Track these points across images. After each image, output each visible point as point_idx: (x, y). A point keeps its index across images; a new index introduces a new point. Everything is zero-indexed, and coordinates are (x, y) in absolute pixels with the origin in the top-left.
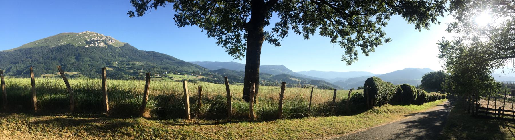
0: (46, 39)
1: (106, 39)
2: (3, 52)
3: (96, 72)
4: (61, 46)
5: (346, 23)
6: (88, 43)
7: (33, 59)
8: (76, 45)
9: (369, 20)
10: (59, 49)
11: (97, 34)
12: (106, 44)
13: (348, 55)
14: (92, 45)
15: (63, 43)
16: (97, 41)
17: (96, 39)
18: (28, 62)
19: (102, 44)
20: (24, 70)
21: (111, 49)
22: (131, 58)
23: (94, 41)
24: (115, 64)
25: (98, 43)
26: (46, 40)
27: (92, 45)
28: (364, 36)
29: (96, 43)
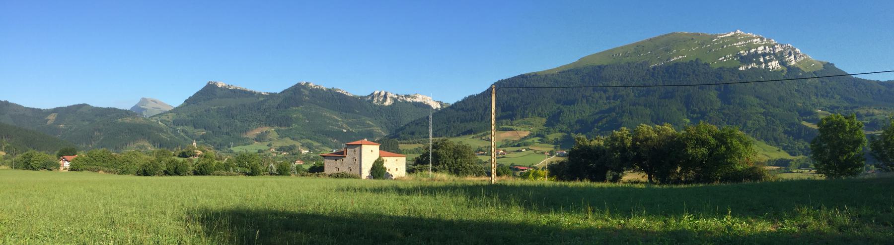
0: (638, 45)
1: (781, 52)
2: (535, 75)
3: (786, 132)
4: (676, 64)
7: (611, 92)
8: (715, 65)
10: (673, 70)
11: (762, 39)
12: (783, 63)
14: (754, 65)
16: (764, 55)
18: (601, 102)
19: (774, 64)
20: (596, 121)
23: (756, 55)
24: (821, 114)
25: (766, 62)
26: (639, 47)
27: (754, 65)
29: (762, 60)
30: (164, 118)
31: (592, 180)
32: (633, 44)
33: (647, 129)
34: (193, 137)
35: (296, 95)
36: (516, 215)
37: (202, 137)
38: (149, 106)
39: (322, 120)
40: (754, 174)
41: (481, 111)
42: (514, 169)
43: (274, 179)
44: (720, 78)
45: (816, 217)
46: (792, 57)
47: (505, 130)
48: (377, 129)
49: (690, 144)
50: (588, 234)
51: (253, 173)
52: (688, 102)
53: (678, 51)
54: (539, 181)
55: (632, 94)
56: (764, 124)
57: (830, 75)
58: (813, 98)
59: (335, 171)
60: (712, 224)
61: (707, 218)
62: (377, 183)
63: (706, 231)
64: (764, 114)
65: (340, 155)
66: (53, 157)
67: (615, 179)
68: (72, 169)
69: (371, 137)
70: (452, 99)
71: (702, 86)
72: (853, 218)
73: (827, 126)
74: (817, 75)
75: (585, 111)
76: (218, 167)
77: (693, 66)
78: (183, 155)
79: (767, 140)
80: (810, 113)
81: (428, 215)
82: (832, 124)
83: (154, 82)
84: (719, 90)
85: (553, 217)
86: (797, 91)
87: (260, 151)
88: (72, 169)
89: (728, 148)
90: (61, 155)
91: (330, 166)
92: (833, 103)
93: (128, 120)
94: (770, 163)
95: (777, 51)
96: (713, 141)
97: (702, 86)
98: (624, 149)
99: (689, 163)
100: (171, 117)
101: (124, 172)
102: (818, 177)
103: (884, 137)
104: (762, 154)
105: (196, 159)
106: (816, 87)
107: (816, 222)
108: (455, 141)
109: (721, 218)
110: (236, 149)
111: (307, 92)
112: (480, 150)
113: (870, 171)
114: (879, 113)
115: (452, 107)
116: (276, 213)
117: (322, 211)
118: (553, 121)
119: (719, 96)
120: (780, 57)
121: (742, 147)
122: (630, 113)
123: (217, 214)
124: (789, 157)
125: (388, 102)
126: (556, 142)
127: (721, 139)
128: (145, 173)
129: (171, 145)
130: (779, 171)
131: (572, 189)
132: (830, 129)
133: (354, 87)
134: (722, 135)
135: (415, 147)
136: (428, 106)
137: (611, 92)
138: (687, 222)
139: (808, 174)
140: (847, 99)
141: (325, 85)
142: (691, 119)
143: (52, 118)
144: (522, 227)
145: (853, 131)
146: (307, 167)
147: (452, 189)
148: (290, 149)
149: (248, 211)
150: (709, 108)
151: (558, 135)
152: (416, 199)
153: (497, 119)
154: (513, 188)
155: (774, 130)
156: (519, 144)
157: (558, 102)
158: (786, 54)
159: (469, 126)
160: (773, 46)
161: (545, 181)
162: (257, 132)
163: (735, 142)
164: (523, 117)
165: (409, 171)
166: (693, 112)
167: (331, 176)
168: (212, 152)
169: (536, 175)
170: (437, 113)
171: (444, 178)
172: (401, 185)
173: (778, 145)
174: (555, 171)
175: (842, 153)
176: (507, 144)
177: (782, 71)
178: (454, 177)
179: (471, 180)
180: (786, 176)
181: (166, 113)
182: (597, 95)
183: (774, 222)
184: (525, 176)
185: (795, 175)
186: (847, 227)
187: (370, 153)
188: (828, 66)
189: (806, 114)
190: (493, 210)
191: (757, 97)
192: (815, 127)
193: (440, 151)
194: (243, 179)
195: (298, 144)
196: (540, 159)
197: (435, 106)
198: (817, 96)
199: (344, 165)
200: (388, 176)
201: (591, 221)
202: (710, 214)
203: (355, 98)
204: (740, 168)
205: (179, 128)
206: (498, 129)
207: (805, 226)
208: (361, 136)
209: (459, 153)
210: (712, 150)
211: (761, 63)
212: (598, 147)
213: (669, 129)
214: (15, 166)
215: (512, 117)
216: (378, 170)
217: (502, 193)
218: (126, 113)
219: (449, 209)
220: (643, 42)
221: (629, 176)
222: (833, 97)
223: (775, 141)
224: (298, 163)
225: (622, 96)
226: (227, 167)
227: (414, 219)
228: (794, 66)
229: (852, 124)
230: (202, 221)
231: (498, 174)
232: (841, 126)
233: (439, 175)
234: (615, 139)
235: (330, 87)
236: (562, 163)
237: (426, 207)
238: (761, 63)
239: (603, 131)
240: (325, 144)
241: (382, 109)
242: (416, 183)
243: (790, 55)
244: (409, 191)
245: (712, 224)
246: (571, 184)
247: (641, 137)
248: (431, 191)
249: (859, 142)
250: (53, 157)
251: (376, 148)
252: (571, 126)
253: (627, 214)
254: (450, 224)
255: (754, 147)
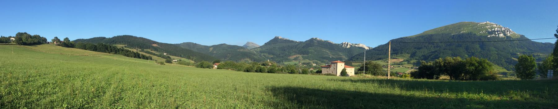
0: (446, 27)
2: (406, 38)
3: (505, 62)
4: (463, 34)
5: (125, 48)
6: (490, 33)
7: (435, 45)
8: (478, 34)
10: (461, 36)
12: (505, 35)
14: (494, 35)
15: (464, 31)
16: (497, 31)
17: (496, 29)
20: (430, 56)
22: (530, 50)
23: (495, 31)
24: (519, 55)
25: (498, 34)
26: (446, 28)
27: (494, 35)
31: (428, 79)
33: (450, 59)
34: (268, 58)
35: (311, 42)
36: (397, 91)
37: (272, 58)
38: (250, 45)
39: (322, 53)
40: (493, 77)
41: (385, 51)
42: (397, 74)
43: (301, 75)
44: (480, 40)
45: (516, 95)
47: (394, 58)
48: (344, 57)
49: (467, 65)
50: (426, 99)
51: (292, 72)
52: (467, 49)
54: (406, 79)
57: (522, 39)
59: (327, 73)
60: (475, 96)
61: (473, 94)
62: (343, 78)
63: (472, 99)
65: (329, 67)
66: (211, 64)
67: (437, 78)
68: (218, 68)
69: (341, 60)
70: (374, 45)
71: (473, 42)
72: (530, 95)
73: (521, 59)
74: (518, 40)
75: (425, 52)
76: (278, 70)
77: (469, 35)
78: (263, 65)
79: (498, 65)
80: (515, 54)
81: (363, 91)
82: (523, 58)
83: (253, 35)
84: (480, 44)
85: (412, 93)
87: (295, 64)
88: (218, 68)
89: (483, 67)
90: (214, 63)
91: (324, 71)
92: (524, 50)
93: (242, 50)
94: (499, 73)
96: (477, 64)
97: (473, 42)
98: (440, 66)
99: (467, 72)
100: (259, 50)
101: (239, 70)
102: (518, 79)
103: (543, 64)
104: (496, 70)
105: (269, 67)
107: (516, 96)
108: (374, 62)
109: (479, 94)
110: (286, 63)
111: (316, 42)
112: (384, 66)
113: (538, 77)
114: (542, 55)
115: (374, 49)
116: (302, 89)
117: (321, 88)
118: (413, 55)
120: (504, 32)
121: (488, 67)
123: (278, 88)
124: (507, 71)
125: (348, 47)
126: (414, 64)
127: (480, 63)
128: (248, 71)
129: (258, 61)
130: (503, 77)
131: (420, 82)
132: (523, 61)
133: (336, 40)
134: (481, 62)
135: (358, 64)
136: (364, 49)
137: (435, 45)
138: (465, 95)
139: (513, 78)
141: (324, 39)
142: (468, 55)
143: (211, 49)
144: (400, 96)
145: (531, 62)
146: (315, 71)
147: (373, 81)
148: (308, 64)
149: (290, 87)
151: (415, 61)
152: (358, 84)
153: (391, 54)
154: (396, 81)
156: (400, 64)
157: (415, 48)
158: (506, 31)
159: (380, 57)
161: (409, 79)
162: (295, 56)
163: (486, 65)
164: (401, 53)
165: (356, 73)
166: (469, 53)
167: (325, 75)
168: (275, 64)
169: (405, 76)
170: (367, 51)
171: (369, 76)
172: (353, 79)
173: (502, 66)
174: (413, 75)
175: (527, 70)
176: (394, 64)
178: (373, 76)
179: (380, 77)
180: (505, 79)
181: (257, 48)
182: (430, 46)
183: (499, 96)
184: (401, 77)
185: (509, 78)
186: (528, 99)
187: (341, 66)
189: (514, 55)
190: (388, 89)
192: (517, 60)
193: (368, 66)
194: (288, 75)
195: (311, 62)
196: (407, 70)
197: (367, 48)
199: (330, 71)
200: (348, 75)
201: (427, 94)
202: (475, 92)
203: (335, 45)
204: (487, 75)
206: (391, 58)
207: (512, 98)
208: (337, 59)
209: (376, 67)
210: (476, 68)
212: (430, 66)
213: (459, 59)
214: (197, 66)
215: (397, 54)
216: (344, 73)
217: (392, 83)
218: (241, 48)
219: (371, 88)
221: (443, 77)
223: (502, 65)
224: (311, 69)
226: (282, 70)
227: (358, 92)
229: (531, 59)
230: (272, 91)
231: (391, 76)
232: (526, 59)
233: (367, 75)
234: (437, 63)
235: (326, 40)
236: (416, 72)
237: (362, 87)
239: (433, 59)
240: (322, 62)
241: (346, 49)
242: (358, 78)
244: (356, 81)
245: (475, 96)
246: (419, 80)
247: (447, 62)
248: (364, 81)
249: (534, 66)
250: (211, 64)
251: (343, 64)
252: (420, 57)
253: (441, 92)
254: (371, 94)
255: (493, 67)
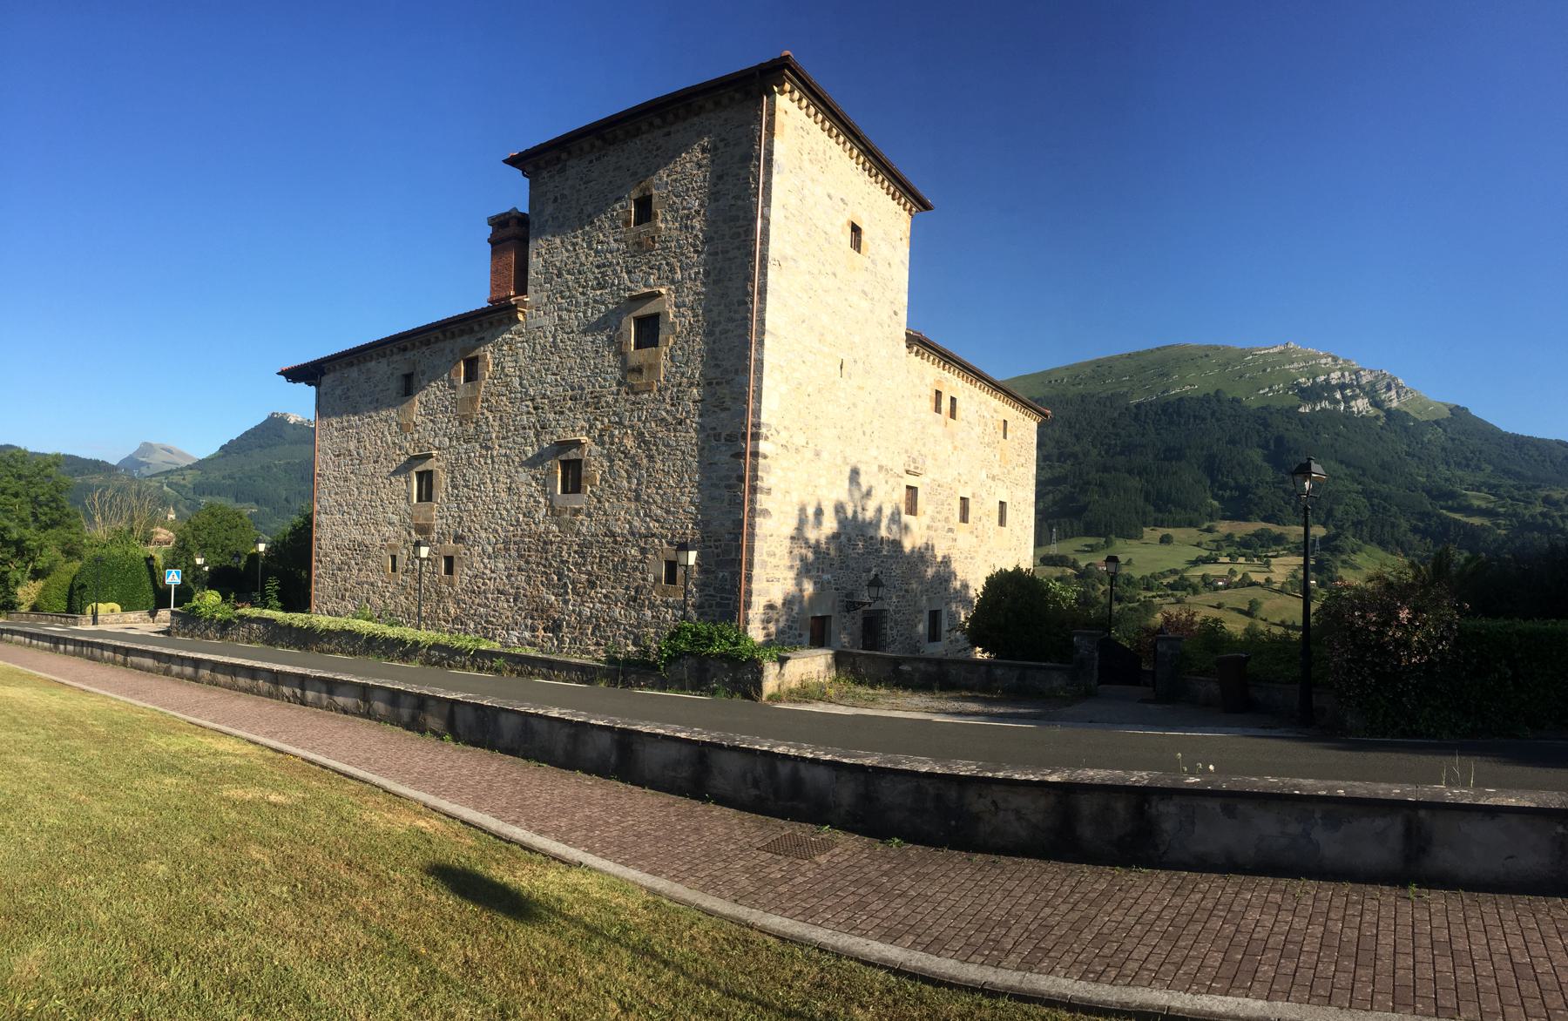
1: (1373, 384)
3: (1415, 530)
8: (1252, 402)
9: (164, 614)
10: (1173, 411)
11: (1335, 359)
12: (1376, 403)
13: (812, 541)
14: (1325, 404)
16: (1342, 387)
17: (1335, 377)
19: (1361, 405)
21: (1406, 429)
23: (1328, 387)
25: (1346, 400)
26: (1100, 369)
27: (1325, 404)
28: (289, 892)
29: (1338, 396)
30: (176, 478)
32: (1091, 363)
44: (1266, 425)
46: (1393, 393)
53: (1182, 377)
55: (1094, 452)
56: (1366, 514)
58: (1442, 468)
64: (1364, 492)
86: (1408, 454)
95: (1364, 381)
100: (190, 478)
102: (756, 612)
106: (1444, 449)
119: (1267, 459)
120: (1371, 393)
122: (1101, 485)
140: (1507, 472)
150: (1254, 481)
155: (1393, 526)
160: (1357, 373)
166: (1223, 487)
177: (1377, 418)
188: (1458, 412)
191: (1341, 462)
198: (1448, 464)
205: (203, 500)
211: (1338, 402)
220: (1110, 359)
222: (1479, 468)
225: (1074, 455)
228: (1397, 410)
238: (1338, 402)
243: (1389, 388)
